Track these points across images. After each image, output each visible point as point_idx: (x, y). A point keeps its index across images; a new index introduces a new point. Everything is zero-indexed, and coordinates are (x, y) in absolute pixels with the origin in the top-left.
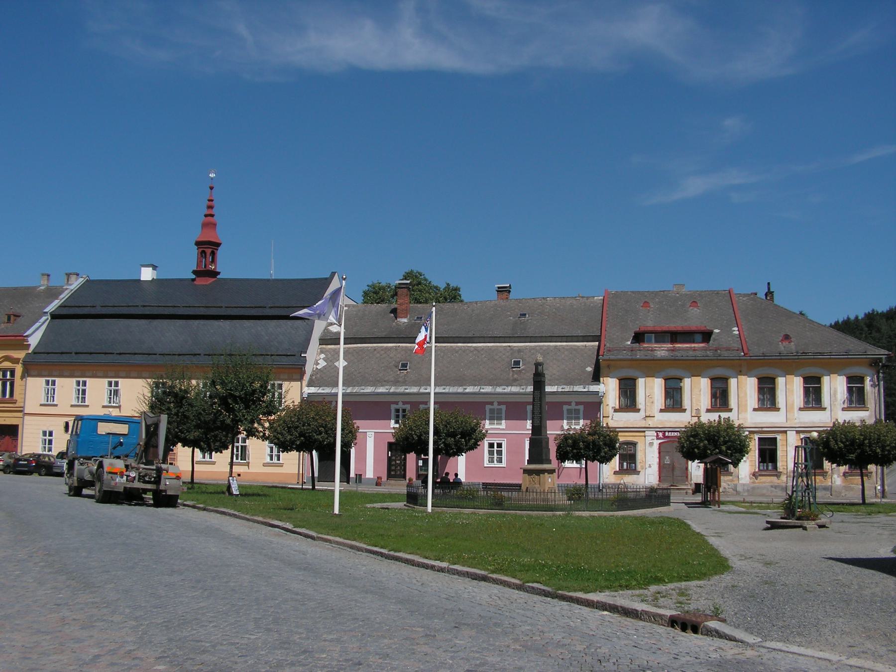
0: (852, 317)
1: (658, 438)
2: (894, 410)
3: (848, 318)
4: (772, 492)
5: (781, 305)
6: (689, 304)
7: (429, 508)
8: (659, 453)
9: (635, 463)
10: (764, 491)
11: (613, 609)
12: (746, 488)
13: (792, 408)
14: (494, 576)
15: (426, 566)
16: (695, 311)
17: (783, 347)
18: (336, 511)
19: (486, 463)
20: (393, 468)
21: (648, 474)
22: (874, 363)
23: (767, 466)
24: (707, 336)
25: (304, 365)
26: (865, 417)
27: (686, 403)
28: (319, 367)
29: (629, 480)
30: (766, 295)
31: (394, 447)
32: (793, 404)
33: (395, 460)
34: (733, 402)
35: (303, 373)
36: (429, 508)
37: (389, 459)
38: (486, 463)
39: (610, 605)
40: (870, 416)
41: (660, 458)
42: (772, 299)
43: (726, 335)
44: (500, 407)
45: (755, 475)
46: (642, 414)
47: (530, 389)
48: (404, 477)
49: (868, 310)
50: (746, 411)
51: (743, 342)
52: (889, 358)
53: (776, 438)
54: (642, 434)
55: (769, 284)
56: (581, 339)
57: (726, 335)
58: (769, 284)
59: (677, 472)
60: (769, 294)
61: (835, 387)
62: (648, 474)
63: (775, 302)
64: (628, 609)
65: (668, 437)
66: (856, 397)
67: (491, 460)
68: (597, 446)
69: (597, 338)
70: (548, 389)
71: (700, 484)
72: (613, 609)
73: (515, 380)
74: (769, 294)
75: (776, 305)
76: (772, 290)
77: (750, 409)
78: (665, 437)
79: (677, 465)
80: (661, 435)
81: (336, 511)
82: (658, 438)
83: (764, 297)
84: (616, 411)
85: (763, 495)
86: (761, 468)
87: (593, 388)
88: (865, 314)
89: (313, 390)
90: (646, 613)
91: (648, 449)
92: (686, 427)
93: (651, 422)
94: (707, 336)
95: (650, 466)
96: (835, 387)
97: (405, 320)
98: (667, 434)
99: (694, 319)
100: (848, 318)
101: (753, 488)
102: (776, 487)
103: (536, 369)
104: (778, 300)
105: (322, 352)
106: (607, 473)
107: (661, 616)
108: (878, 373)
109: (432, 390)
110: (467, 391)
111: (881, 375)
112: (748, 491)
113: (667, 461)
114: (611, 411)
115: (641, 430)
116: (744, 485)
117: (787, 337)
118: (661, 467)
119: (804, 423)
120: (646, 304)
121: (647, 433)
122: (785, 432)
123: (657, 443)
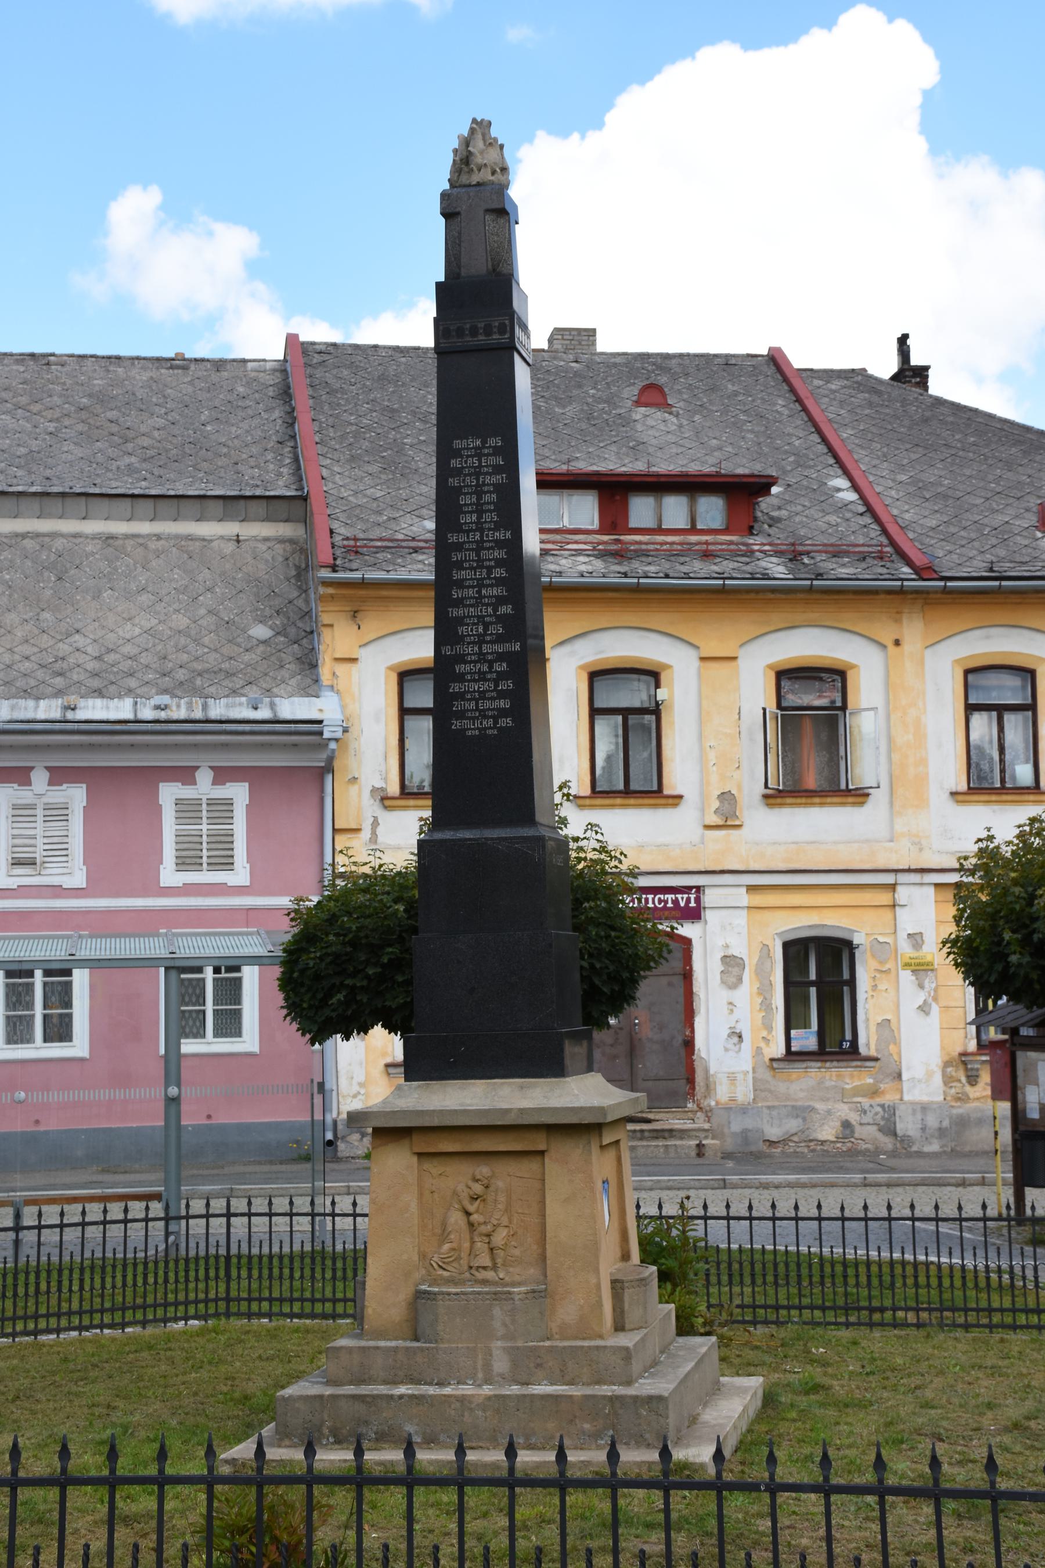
5: (61, 348)
12: (932, 1121)
16: (650, 423)
27: (679, 774)
50: (921, 802)
55: (903, 340)
76: (915, 360)
87: (294, 707)
110: (81, 715)
112: (942, 1132)
114: (370, 808)
116: (925, 1108)
122: (893, 887)
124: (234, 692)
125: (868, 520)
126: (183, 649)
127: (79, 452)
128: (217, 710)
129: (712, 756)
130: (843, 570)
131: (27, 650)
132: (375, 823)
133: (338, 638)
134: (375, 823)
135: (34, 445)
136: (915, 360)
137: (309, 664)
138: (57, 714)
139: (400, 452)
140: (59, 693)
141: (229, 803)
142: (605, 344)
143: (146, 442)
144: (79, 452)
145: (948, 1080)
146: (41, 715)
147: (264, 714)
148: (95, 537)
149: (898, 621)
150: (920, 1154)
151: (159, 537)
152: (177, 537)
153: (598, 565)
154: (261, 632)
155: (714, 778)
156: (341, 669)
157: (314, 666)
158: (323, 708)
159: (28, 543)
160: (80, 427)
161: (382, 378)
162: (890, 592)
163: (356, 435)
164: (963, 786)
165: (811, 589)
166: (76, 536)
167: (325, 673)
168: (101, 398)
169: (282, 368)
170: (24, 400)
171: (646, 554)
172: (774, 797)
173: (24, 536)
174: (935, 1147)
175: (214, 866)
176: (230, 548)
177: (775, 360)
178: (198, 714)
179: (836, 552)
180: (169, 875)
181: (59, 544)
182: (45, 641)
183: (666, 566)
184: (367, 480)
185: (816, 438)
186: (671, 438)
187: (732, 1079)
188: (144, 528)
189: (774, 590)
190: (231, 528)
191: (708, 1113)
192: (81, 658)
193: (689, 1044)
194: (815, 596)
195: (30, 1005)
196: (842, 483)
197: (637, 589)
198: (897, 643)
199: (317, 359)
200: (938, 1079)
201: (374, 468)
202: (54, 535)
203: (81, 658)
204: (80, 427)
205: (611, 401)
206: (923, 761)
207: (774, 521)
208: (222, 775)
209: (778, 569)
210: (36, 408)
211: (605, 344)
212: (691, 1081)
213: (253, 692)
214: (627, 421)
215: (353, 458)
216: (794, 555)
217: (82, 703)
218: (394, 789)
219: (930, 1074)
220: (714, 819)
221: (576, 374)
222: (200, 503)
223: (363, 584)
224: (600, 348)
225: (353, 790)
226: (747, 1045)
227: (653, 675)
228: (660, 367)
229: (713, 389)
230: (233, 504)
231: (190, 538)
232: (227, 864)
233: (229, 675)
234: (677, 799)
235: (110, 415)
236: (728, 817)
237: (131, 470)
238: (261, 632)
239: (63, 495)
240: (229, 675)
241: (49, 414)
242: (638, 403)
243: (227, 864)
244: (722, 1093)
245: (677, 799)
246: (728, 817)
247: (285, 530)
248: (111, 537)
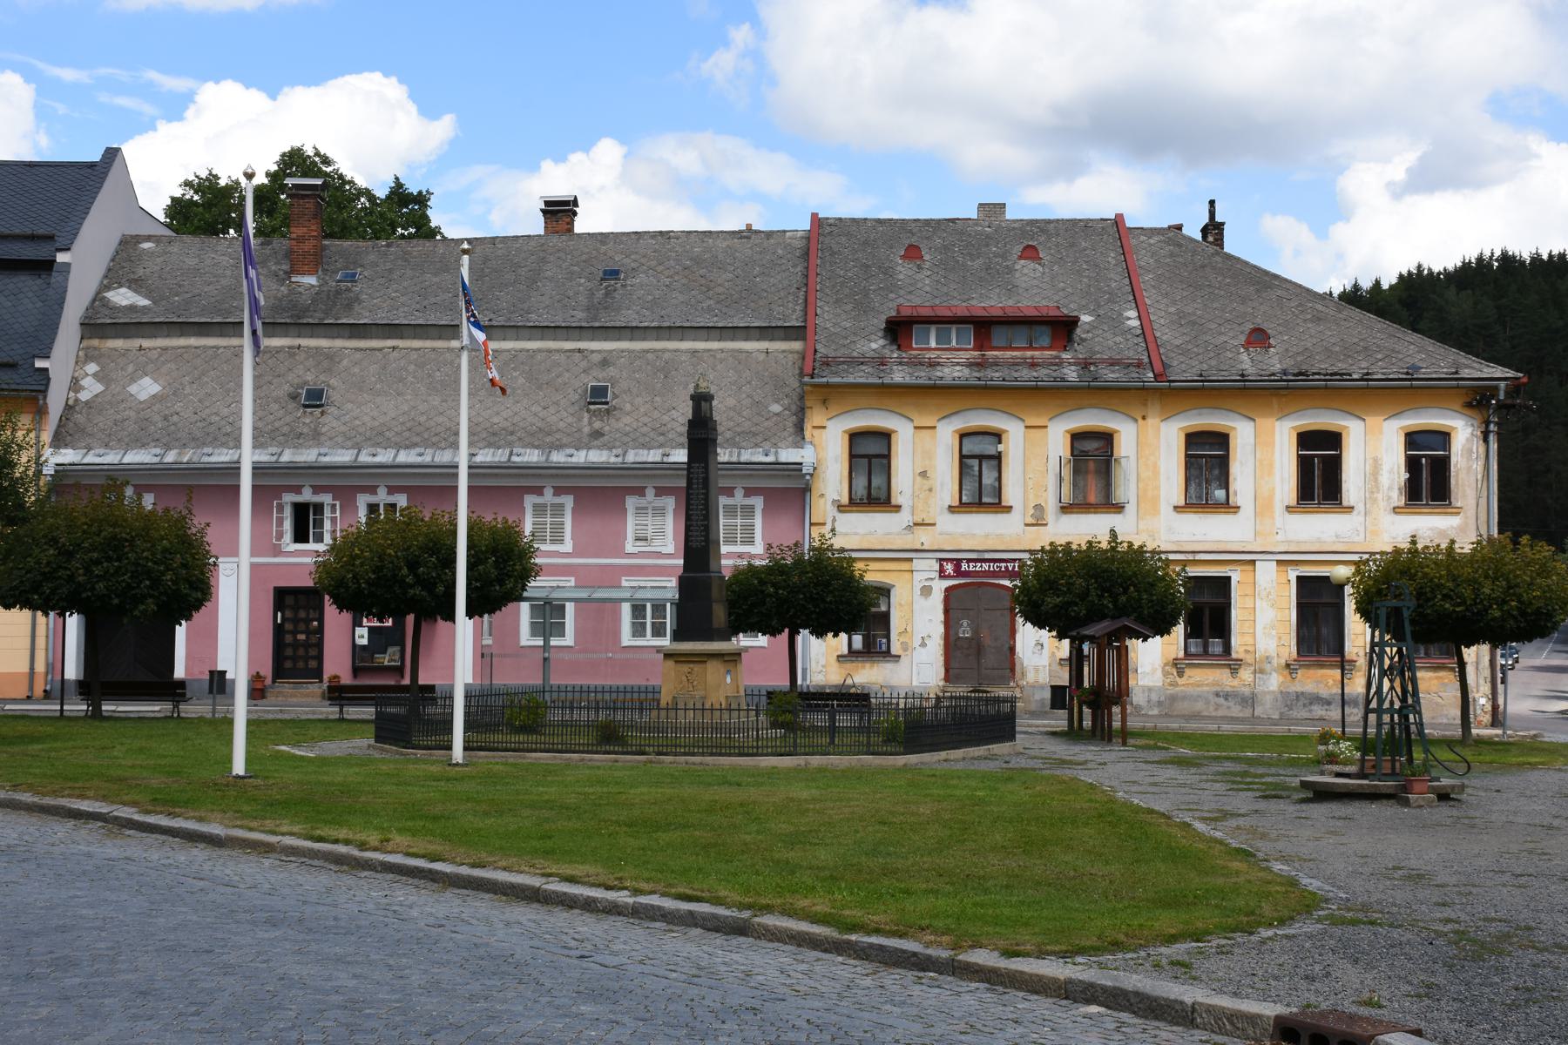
0: (1366, 284)
1: (942, 575)
2: (1519, 506)
3: (1356, 287)
4: (1218, 706)
5: (677, 228)
6: (1018, 249)
7: (458, 752)
8: (946, 611)
9: (888, 637)
10: (1199, 706)
11: (1116, 999)
12: (1154, 697)
13: (1155, 501)
14: (770, 920)
15: (569, 903)
16: (1026, 270)
17: (1247, 362)
18: (239, 768)
19: (627, 639)
20: (289, 652)
21: (917, 666)
22: (1477, 400)
23: (1206, 646)
24: (1063, 329)
25: (45, 392)
26: (1462, 524)
27: (1011, 494)
28: (84, 396)
29: (868, 676)
30: (1205, 231)
31: (289, 600)
32: (1271, 498)
33: (294, 633)
34: (1126, 486)
35: (41, 412)
36: (458, 752)
37: (278, 631)
38: (627, 639)
39: (1104, 989)
40: (1462, 529)
41: (947, 623)
42: (1219, 242)
43: (1110, 331)
44: (558, 500)
45: (1178, 666)
46: (904, 518)
47: (681, 456)
48: (318, 674)
49: (1406, 265)
50: (1155, 511)
51: (1152, 346)
52: (1515, 389)
53: (1227, 581)
54: (905, 566)
55: (1212, 203)
56: (781, 333)
57: (1110, 331)
58: (1212, 203)
59: (990, 659)
60: (1214, 230)
61: (1374, 449)
62: (917, 666)
63: (1226, 249)
64: (1156, 999)
65: (967, 574)
66: (1428, 480)
67: (638, 630)
68: (833, 597)
69: (797, 332)
70: (724, 455)
71: (1064, 687)
72: (1116, 999)
73: (597, 434)
74: (1214, 230)
75: (1229, 257)
76: (1218, 219)
77: (1279, 508)
78: (959, 573)
79: (987, 641)
80: (949, 568)
81: (239, 768)
82: (942, 575)
83: (1199, 237)
84: (841, 508)
85: (1196, 716)
86: (1193, 650)
87: (788, 455)
88: (1401, 276)
89: (68, 456)
90: (1210, 1009)
91: (920, 603)
92: (1043, 550)
93: (924, 538)
94: (1063, 329)
95: (923, 645)
96: (1374, 449)
97: (311, 280)
98: (964, 566)
99: (1032, 289)
100: (1356, 287)
101: (1173, 699)
102: (1227, 696)
103: (697, 409)
104: (1231, 245)
105: (89, 358)
106: (823, 659)
107: (1253, 1019)
108: (1487, 423)
109: (248, 457)
110: (671, 459)
111: (1492, 427)
112: (1160, 703)
113: (965, 631)
114: (831, 511)
115: (904, 556)
116: (1150, 689)
117: (1258, 338)
118: (951, 645)
119: (1319, 541)
120: (913, 253)
121: (917, 564)
122: (1253, 562)
123: (940, 586)
124: (757, 445)
125: (1141, 339)
126: (731, 419)
127: (681, 298)
128: (746, 456)
129: (1030, 483)
130: (1111, 375)
131: (646, 420)
132: (834, 520)
133: (815, 417)
134: (834, 520)
135: (657, 293)
136: (1218, 219)
137: (799, 428)
138: (658, 459)
139: (867, 295)
140: (661, 446)
141: (752, 507)
142: (1010, 215)
143: (720, 290)
144: (681, 298)
145: (1166, 674)
146: (650, 459)
147: (770, 459)
148: (687, 351)
149: (1145, 405)
150: (1146, 715)
151: (722, 351)
152: (733, 350)
153: (966, 371)
154: (776, 408)
155: (1031, 496)
156: (816, 432)
157: (802, 429)
158: (804, 456)
159: (650, 356)
160: (684, 281)
161: (866, 243)
162: (1137, 389)
163: (842, 284)
164: (1182, 503)
165: (1089, 387)
166: (676, 351)
167: (807, 434)
168: (697, 261)
169: (808, 237)
170: (653, 263)
171: (996, 364)
172: (1066, 509)
173: (648, 351)
174: (1155, 712)
175: (553, 542)
176: (762, 357)
177: (1118, 221)
178: (734, 459)
179: (1113, 363)
180: (630, 547)
181: (667, 356)
182: (656, 414)
183: (1006, 371)
184: (844, 316)
185: (1127, 281)
186: (1036, 282)
187: (1037, 669)
188: (715, 345)
189: (1068, 388)
190: (764, 345)
191: (1022, 688)
192: (675, 425)
193: (1012, 650)
194: (1092, 392)
195: (644, 617)
196: (1133, 313)
197: (986, 387)
198: (1144, 418)
199: (828, 229)
200: (1159, 674)
201: (849, 307)
202: (664, 351)
203: (675, 425)
204: (684, 281)
205: (1004, 256)
206: (1158, 488)
207: (1084, 340)
208: (749, 492)
209: (1072, 374)
210: (660, 268)
211: (1010, 215)
212: (1013, 670)
213: (767, 445)
214: (1010, 270)
215: (837, 301)
216: (1085, 365)
217: (673, 452)
218: (845, 500)
219: (1154, 671)
220: (1030, 520)
221: (988, 236)
222: (746, 332)
223: (827, 385)
224: (1009, 216)
225: (822, 501)
226: (1046, 651)
227: (997, 436)
228: (1042, 231)
229: (1072, 245)
230: (766, 332)
231: (740, 351)
232: (751, 542)
233: (755, 434)
234: (1009, 509)
235: (702, 272)
236: (1038, 521)
237: (710, 309)
238: (776, 408)
239: (670, 328)
240: (755, 434)
241: (667, 273)
242: (1020, 258)
243: (751, 542)
244: (1031, 677)
245: (1009, 509)
246: (1038, 521)
247: (797, 345)
248: (696, 351)
